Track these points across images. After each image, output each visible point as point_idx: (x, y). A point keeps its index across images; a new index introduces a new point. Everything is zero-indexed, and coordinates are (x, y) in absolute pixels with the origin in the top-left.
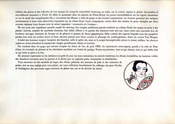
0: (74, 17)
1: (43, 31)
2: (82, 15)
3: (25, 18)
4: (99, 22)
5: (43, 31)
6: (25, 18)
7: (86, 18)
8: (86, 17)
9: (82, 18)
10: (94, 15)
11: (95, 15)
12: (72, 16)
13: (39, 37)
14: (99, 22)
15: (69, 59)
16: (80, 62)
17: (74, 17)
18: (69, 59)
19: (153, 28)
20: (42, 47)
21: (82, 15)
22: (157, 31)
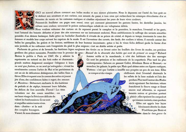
0: (21, 82)
1: (113, 36)
2: (29, 53)
3: (135, 33)
4: (143, 17)
5: (113, 36)
6: (135, 33)
7: (44, 70)
8: (47, 61)
9: (60, 73)
10: (39, 57)
11: (40, 57)
12: (142, 35)
13: (51, 26)
14: (143, 17)
15: (93, 23)
16: (121, 39)
17: (21, 82)
18: (93, 23)
19: (48, 80)
20: (66, 23)
21: (29, 53)
22: (72, 70)
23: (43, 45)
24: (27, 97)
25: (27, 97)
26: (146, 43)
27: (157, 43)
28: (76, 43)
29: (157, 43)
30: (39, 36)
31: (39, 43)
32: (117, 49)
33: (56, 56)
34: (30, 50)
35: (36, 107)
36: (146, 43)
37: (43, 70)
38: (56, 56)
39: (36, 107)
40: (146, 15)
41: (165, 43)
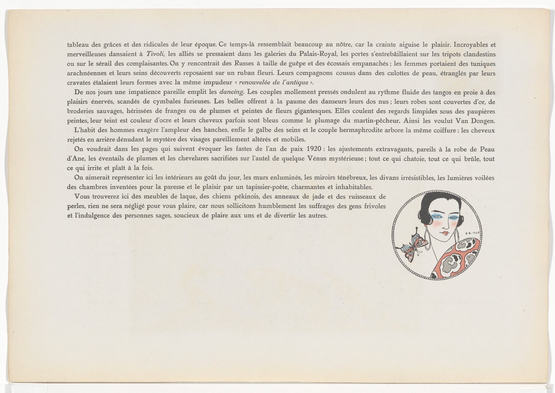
7: (177, 140)
23: (215, 116)
24: (200, 140)
25: (200, 140)
26: (351, 207)
27: (186, 159)
28: (203, 111)
29: (186, 159)
30: (240, 150)
31: (175, 54)
32: (469, 119)
33: (77, 149)
34: (132, 159)
35: (449, 150)
36: (351, 207)
37: (113, 140)
38: (77, 149)
39: (449, 150)
40: (374, 154)
41: (69, 45)
